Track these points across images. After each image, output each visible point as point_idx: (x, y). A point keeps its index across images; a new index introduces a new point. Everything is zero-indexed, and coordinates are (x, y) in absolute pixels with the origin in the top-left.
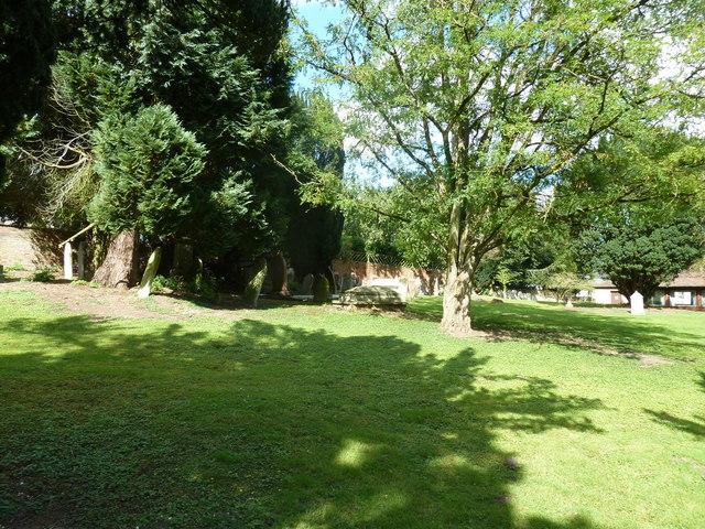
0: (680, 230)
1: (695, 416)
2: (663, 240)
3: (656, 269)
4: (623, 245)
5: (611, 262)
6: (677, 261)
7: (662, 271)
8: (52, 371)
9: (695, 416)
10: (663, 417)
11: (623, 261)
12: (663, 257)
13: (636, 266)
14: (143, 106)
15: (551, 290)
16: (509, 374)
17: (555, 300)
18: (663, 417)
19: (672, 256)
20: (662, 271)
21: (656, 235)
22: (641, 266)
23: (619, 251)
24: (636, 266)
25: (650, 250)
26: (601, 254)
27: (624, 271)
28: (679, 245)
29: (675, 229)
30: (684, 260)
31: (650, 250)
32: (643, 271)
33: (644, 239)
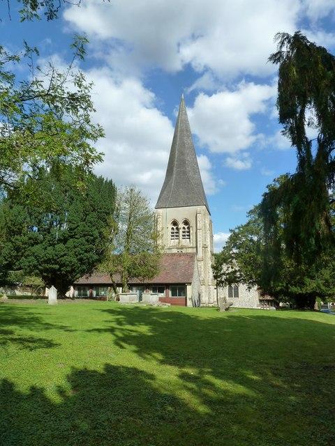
0: (87, 241)
1: (50, 344)
2: (75, 247)
3: (69, 269)
4: (45, 249)
5: (35, 262)
6: (84, 264)
7: (73, 270)
8: (225, 268)
9: (50, 344)
10: (89, 331)
11: (45, 262)
12: (75, 260)
13: (54, 266)
14: (243, 81)
15: (28, 286)
16: (62, 332)
17: (29, 294)
18: (89, 331)
19: (81, 260)
20: (73, 270)
21: (71, 242)
22: (57, 267)
23: (42, 253)
24: (54, 266)
25: (65, 255)
26: (28, 255)
27: (46, 270)
28: (86, 251)
29: (83, 240)
30: (89, 263)
31: (65, 255)
32: (59, 270)
33: (61, 245)
